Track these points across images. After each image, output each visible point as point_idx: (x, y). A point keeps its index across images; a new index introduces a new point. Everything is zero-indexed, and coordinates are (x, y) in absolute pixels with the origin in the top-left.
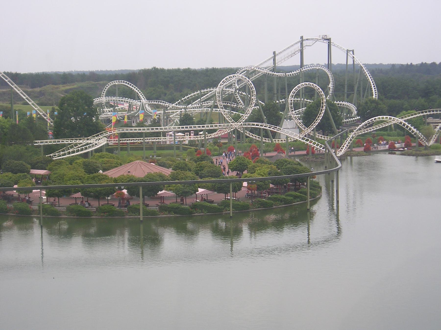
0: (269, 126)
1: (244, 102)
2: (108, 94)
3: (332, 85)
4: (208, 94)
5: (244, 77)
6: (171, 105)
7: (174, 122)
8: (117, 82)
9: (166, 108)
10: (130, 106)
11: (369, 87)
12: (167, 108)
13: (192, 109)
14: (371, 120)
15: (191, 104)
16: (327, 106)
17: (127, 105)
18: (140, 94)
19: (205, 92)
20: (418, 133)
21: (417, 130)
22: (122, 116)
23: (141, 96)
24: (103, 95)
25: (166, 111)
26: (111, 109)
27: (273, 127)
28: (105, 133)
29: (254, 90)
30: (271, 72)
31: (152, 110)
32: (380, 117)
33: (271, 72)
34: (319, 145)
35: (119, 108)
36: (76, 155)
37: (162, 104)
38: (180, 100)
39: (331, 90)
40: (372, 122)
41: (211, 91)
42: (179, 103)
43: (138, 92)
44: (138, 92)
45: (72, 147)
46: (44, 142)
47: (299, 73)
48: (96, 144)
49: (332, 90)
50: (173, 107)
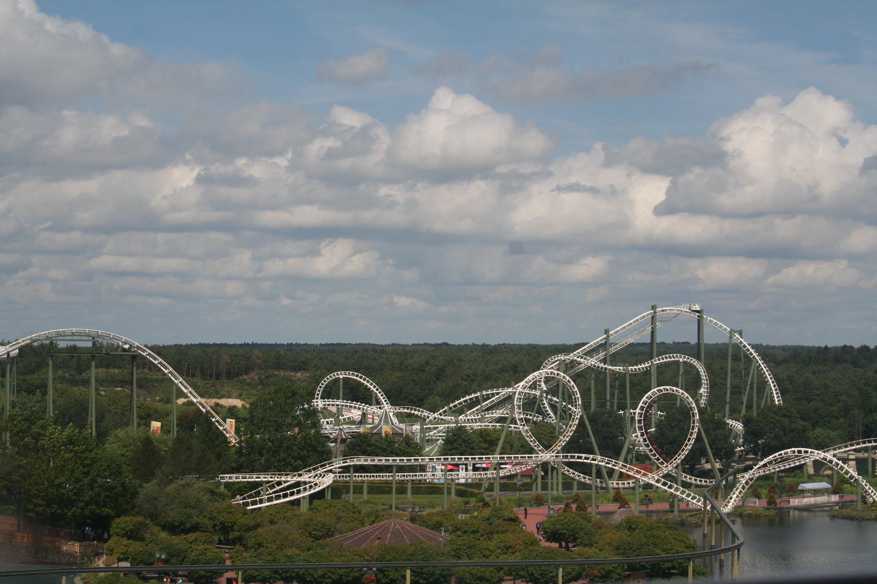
0: (606, 461)
1: (555, 414)
2: (327, 395)
3: (706, 390)
4: (493, 399)
5: (556, 372)
6: (432, 416)
7: (437, 444)
8: (341, 374)
9: (423, 420)
10: (364, 415)
11: (769, 395)
12: (425, 420)
13: (473, 423)
14: (779, 455)
15: (464, 415)
16: (701, 427)
17: (358, 414)
18: (379, 395)
19: (488, 394)
20: (860, 479)
21: (858, 475)
22: (350, 432)
23: (381, 398)
24: (318, 395)
25: (425, 426)
26: (331, 419)
27: (613, 463)
28: (329, 464)
29: (578, 398)
30: (602, 365)
31: (400, 423)
32: (801, 451)
33: (602, 365)
34: (691, 495)
35: (345, 418)
36: (282, 503)
37: (416, 413)
38: (446, 408)
39: (703, 398)
40: (780, 458)
41: (498, 394)
42: (445, 412)
43: (377, 392)
44: (376, 391)
45: (273, 487)
46: (227, 477)
47: (650, 366)
48: (316, 485)
49: (705, 398)
50: (435, 418)
